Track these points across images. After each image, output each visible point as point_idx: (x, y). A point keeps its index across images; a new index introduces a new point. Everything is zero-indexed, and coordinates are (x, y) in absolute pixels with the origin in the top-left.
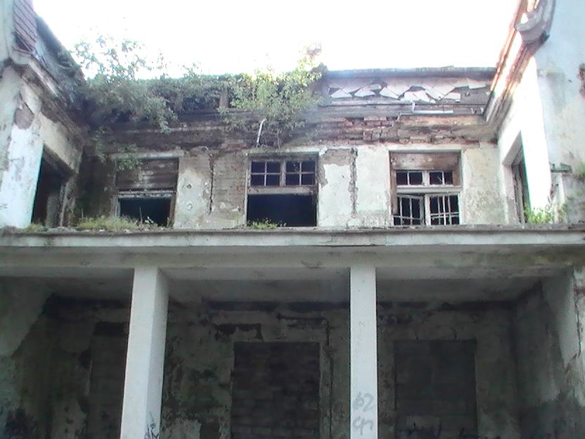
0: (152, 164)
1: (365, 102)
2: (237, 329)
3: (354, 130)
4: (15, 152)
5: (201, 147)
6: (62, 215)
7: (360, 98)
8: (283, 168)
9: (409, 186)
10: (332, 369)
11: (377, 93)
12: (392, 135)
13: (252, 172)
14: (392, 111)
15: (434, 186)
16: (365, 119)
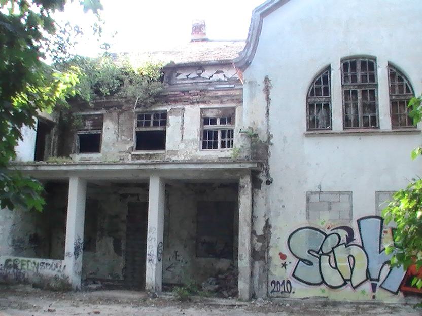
1: (192, 81)
3: (184, 97)
6: (52, 144)
8: (152, 118)
9: (210, 125)
11: (199, 75)
14: (205, 86)
15: (222, 125)
16: (190, 92)
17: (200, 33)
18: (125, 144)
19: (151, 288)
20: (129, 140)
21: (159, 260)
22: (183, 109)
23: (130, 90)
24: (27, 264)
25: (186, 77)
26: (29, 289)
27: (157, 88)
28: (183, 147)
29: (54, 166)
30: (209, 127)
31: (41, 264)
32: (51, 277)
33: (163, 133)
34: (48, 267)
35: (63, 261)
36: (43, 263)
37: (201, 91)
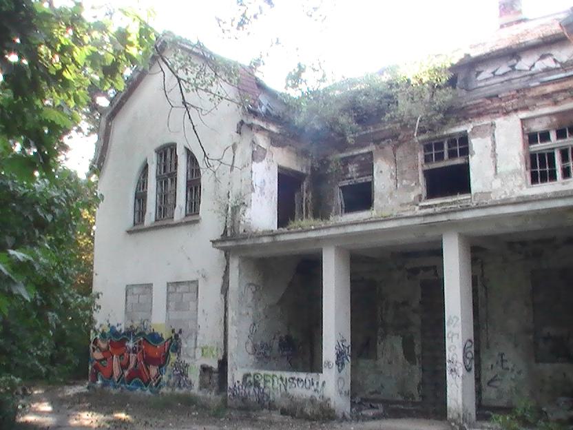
0: (356, 159)
1: (502, 79)
2: (422, 271)
3: (494, 106)
4: (257, 180)
5: (387, 140)
6: (304, 205)
7: (500, 75)
10: (486, 294)
11: (513, 67)
12: (521, 105)
13: (425, 151)
16: (500, 96)
17: (512, 12)
18: (408, 191)
19: (456, 415)
20: (413, 184)
21: (469, 370)
22: (493, 125)
23: (404, 106)
24: (271, 380)
25: (492, 75)
26: (276, 416)
27: (446, 96)
28: (500, 186)
29: (306, 231)
30: (539, 146)
31: (291, 380)
32: (305, 400)
33: (464, 170)
34: (301, 385)
35: (320, 374)
36: (293, 379)
37: (518, 91)
